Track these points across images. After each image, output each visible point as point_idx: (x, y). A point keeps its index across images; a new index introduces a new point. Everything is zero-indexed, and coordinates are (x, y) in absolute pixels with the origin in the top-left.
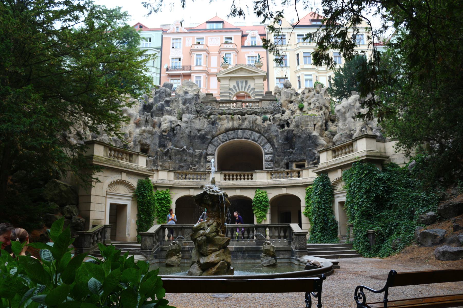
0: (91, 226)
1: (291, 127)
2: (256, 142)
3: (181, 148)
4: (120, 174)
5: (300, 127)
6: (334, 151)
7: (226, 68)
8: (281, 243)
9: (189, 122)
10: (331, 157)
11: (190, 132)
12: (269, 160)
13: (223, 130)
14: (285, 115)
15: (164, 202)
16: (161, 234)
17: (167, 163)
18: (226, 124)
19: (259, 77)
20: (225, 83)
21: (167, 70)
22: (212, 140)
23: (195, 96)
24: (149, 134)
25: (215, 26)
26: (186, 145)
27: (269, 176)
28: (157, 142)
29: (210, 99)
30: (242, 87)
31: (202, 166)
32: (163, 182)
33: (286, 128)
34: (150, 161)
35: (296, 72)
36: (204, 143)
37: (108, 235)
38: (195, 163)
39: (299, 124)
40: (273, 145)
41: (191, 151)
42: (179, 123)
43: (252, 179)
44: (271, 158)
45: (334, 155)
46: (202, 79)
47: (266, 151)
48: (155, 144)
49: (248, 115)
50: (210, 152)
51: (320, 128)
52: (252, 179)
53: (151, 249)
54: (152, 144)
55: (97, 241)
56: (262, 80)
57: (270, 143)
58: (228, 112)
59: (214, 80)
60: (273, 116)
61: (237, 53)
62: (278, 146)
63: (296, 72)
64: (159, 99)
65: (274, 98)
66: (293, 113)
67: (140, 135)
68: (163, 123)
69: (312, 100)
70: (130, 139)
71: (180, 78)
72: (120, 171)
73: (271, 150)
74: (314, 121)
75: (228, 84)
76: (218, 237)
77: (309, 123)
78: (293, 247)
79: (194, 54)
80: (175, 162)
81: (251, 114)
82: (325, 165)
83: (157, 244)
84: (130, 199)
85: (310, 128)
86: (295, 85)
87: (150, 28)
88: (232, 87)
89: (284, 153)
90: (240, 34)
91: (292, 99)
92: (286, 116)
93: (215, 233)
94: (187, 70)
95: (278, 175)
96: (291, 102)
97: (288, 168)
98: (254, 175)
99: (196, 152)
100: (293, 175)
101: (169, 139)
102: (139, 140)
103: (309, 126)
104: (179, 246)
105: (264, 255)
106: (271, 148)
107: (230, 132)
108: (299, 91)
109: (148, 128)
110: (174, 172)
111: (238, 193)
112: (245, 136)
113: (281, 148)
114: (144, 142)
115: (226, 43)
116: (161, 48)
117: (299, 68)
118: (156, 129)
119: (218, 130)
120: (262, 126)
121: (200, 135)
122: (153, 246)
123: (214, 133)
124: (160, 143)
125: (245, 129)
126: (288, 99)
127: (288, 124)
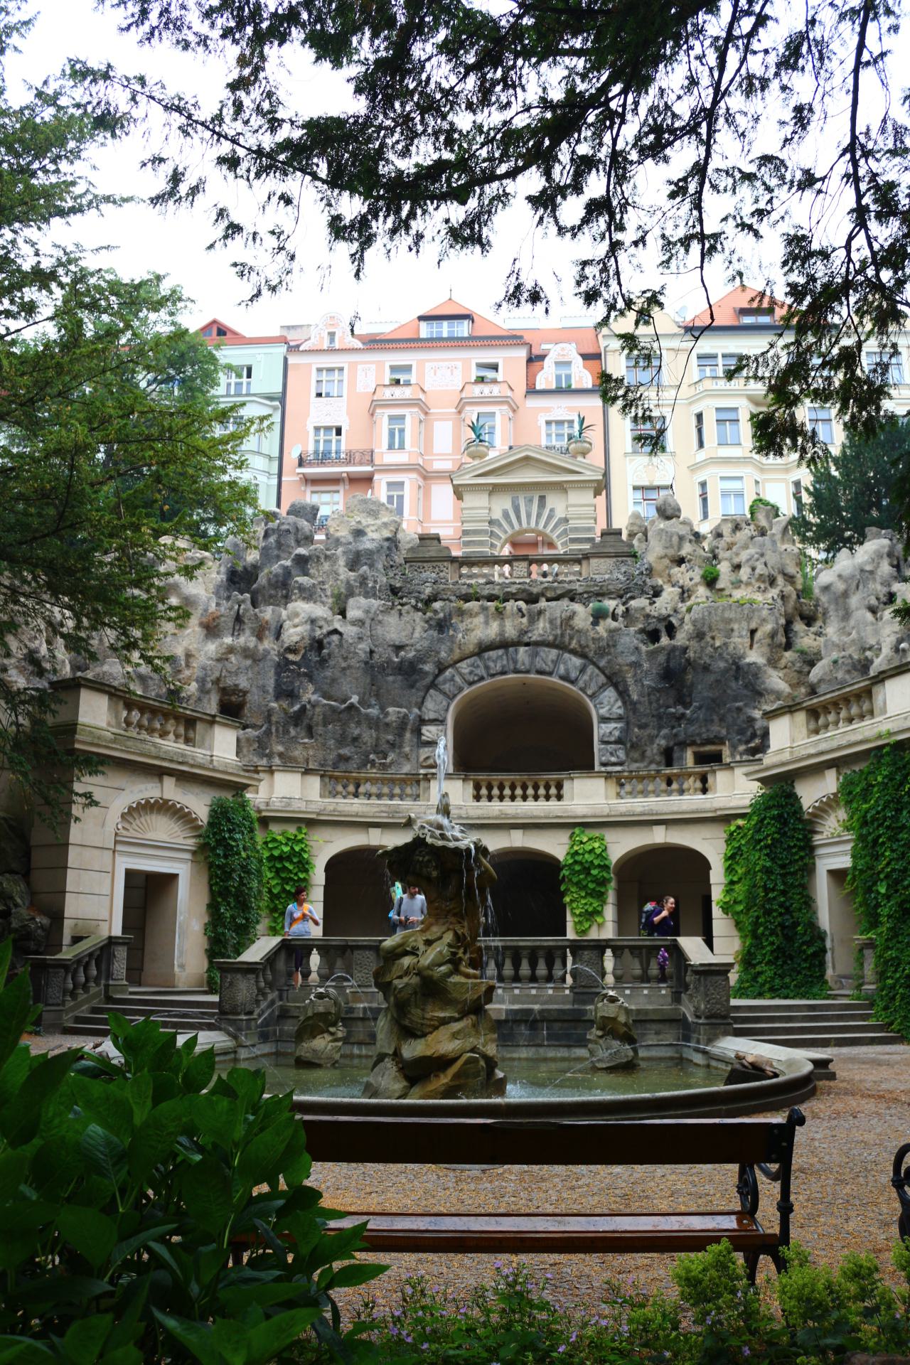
0: (66, 939)
1: (681, 638)
2: (572, 682)
3: (344, 701)
6: (814, 713)
7: (482, 456)
8: (650, 999)
9: (368, 622)
10: (804, 731)
11: (372, 652)
12: (612, 739)
13: (471, 648)
15: (291, 867)
17: (300, 748)
18: (479, 627)
19: (582, 485)
20: (478, 503)
21: (301, 462)
22: (437, 676)
24: (246, 657)
25: (445, 329)
26: (358, 694)
27: (613, 788)
28: (271, 683)
29: (432, 552)
30: (529, 516)
31: (407, 757)
32: (289, 805)
33: (664, 640)
35: (694, 468)
36: (412, 686)
38: (385, 747)
39: (706, 629)
40: (623, 694)
42: (337, 626)
43: (559, 797)
44: (617, 733)
45: (812, 726)
47: (603, 711)
48: (263, 689)
49: (548, 600)
50: (432, 716)
51: (768, 641)
52: (559, 797)
53: (250, 1013)
54: (254, 690)
55: (85, 987)
57: (616, 686)
58: (486, 592)
59: (443, 494)
60: (624, 604)
61: (514, 411)
62: (641, 695)
64: (276, 552)
65: (626, 549)
66: (685, 594)
67: (218, 660)
68: (287, 624)
69: (744, 556)
70: (187, 673)
72: (159, 773)
73: (618, 709)
74: (749, 619)
75: (487, 505)
76: (456, 979)
77: (736, 626)
78: (687, 1010)
79: (383, 415)
80: (324, 745)
81: (557, 598)
82: (786, 756)
83: (270, 997)
84: (188, 856)
85: (739, 641)
88: (497, 515)
89: (660, 717)
90: (522, 354)
91: (683, 553)
92: (666, 602)
94: (361, 464)
95: (640, 787)
96: (680, 561)
97: (669, 763)
98: (566, 785)
99: (387, 714)
100: (685, 786)
101: (305, 674)
102: (213, 677)
103: (736, 633)
105: (600, 1033)
106: (619, 703)
108: (705, 528)
109: (242, 640)
110: (322, 776)
111: (518, 840)
113: (650, 703)
114: (230, 682)
115: (481, 380)
117: (702, 455)
118: (268, 644)
120: (592, 634)
121: (401, 662)
122: (257, 1002)
123: (443, 654)
124: (278, 685)
125: (538, 644)
126: (671, 552)
127: (671, 630)
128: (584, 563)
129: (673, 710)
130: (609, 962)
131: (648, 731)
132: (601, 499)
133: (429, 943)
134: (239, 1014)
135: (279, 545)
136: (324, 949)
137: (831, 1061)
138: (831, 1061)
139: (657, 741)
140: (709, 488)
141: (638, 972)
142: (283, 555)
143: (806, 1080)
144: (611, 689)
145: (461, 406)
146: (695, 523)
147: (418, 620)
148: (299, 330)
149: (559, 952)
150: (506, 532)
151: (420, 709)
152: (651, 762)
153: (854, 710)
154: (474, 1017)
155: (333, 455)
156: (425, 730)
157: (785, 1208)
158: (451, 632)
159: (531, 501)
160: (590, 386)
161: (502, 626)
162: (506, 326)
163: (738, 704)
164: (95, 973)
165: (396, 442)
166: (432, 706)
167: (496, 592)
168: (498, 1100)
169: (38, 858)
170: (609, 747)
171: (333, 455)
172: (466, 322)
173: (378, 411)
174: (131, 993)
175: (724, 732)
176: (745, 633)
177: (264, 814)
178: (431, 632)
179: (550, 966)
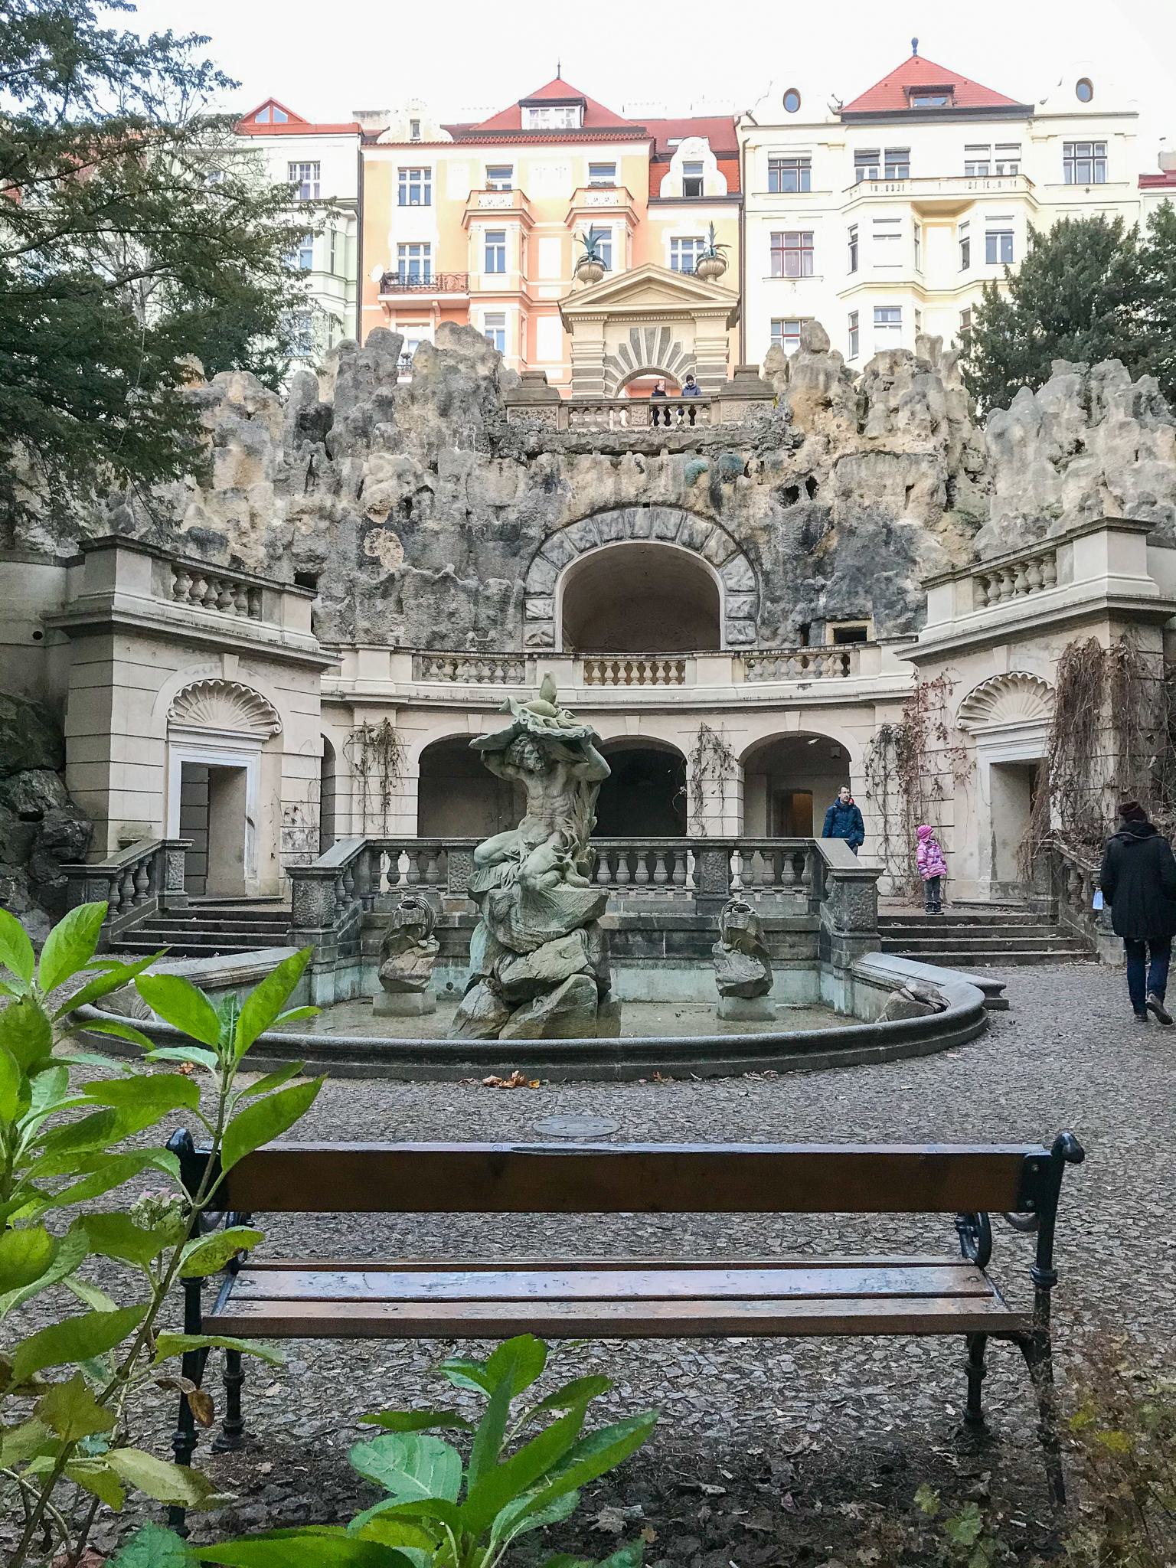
0: (112, 844)
2: (697, 549)
3: (437, 570)
4: (215, 658)
5: (855, 496)
7: (596, 278)
8: (785, 906)
9: (463, 477)
10: (970, 602)
11: (468, 513)
12: (741, 615)
13: (583, 509)
14: (801, 454)
16: (365, 870)
18: (591, 482)
19: (711, 314)
20: (588, 334)
21: (385, 284)
22: (543, 542)
23: (484, 384)
24: (322, 517)
25: (554, 119)
27: (741, 670)
29: (538, 393)
31: (510, 635)
33: (804, 500)
34: (328, 614)
35: (843, 294)
36: (515, 555)
37: (176, 875)
39: (854, 486)
40: (754, 562)
41: (472, 583)
42: (428, 481)
43: (680, 680)
44: (746, 608)
45: (981, 596)
46: (511, 326)
47: (731, 584)
49: (670, 453)
51: (927, 499)
52: (680, 680)
53: (330, 925)
54: (333, 556)
55: (135, 898)
56: (723, 323)
57: (746, 553)
58: (599, 443)
59: (549, 326)
60: (759, 456)
61: (634, 225)
62: (775, 563)
63: (843, 294)
64: (353, 392)
65: (763, 390)
68: (367, 481)
71: (432, 315)
72: (218, 650)
73: (748, 582)
75: (601, 339)
76: (563, 888)
77: (889, 482)
78: (828, 919)
79: (479, 228)
81: (681, 451)
83: (352, 906)
85: (892, 500)
86: (839, 342)
87: (313, 122)
88: (613, 351)
89: (796, 589)
90: (643, 150)
93: (556, 873)
94: (454, 291)
95: (772, 668)
96: (828, 404)
98: (688, 665)
99: (487, 586)
100: (823, 668)
102: (285, 541)
103: (888, 491)
104: (427, 913)
105: (728, 946)
107: (607, 516)
108: (857, 366)
111: (632, 727)
112: (658, 528)
113: (786, 573)
116: (359, 206)
118: (344, 502)
119: (564, 508)
122: (337, 912)
123: (550, 517)
127: (811, 485)
128: (713, 406)
129: (811, 581)
130: (736, 864)
131: (782, 605)
132: (734, 332)
133: (532, 846)
134: (315, 927)
135: (357, 384)
136: (417, 852)
137: (1004, 987)
138: (1004, 987)
139: (792, 617)
140: (860, 320)
141: (770, 877)
142: (361, 395)
143: (976, 1014)
144: (741, 556)
145: (571, 219)
146: (846, 356)
147: (521, 475)
148: (376, 118)
149: (679, 854)
150: (623, 372)
151: (524, 580)
152: (785, 640)
153: (1033, 577)
154: (583, 932)
155: (422, 279)
156: (530, 604)
157: (1045, 1278)
158: (560, 491)
159: (653, 333)
160: (724, 193)
161: (618, 483)
162: (626, 116)
163: (885, 574)
164: (147, 882)
165: (494, 263)
166: (539, 576)
167: (611, 443)
168: (612, 1040)
169: (75, 751)
170: (737, 623)
171: (422, 279)
172: (577, 108)
173: (473, 223)
174: (191, 904)
175: (870, 605)
176: (902, 490)
177: (348, 698)
178: (537, 490)
179: (670, 870)
